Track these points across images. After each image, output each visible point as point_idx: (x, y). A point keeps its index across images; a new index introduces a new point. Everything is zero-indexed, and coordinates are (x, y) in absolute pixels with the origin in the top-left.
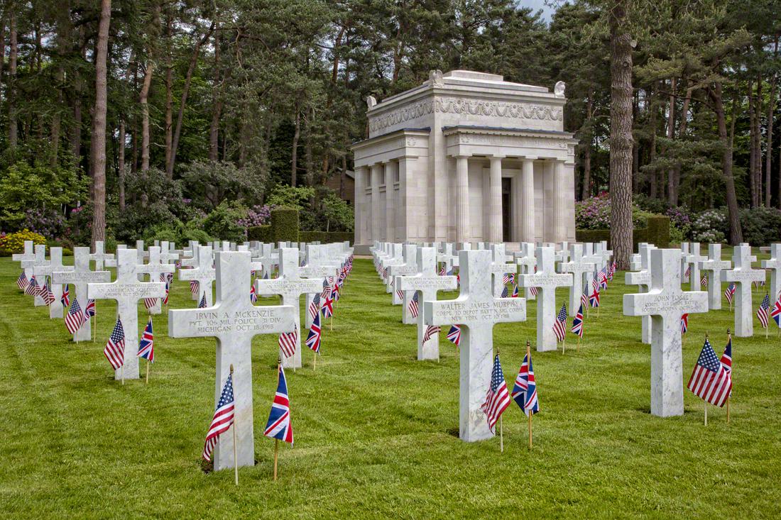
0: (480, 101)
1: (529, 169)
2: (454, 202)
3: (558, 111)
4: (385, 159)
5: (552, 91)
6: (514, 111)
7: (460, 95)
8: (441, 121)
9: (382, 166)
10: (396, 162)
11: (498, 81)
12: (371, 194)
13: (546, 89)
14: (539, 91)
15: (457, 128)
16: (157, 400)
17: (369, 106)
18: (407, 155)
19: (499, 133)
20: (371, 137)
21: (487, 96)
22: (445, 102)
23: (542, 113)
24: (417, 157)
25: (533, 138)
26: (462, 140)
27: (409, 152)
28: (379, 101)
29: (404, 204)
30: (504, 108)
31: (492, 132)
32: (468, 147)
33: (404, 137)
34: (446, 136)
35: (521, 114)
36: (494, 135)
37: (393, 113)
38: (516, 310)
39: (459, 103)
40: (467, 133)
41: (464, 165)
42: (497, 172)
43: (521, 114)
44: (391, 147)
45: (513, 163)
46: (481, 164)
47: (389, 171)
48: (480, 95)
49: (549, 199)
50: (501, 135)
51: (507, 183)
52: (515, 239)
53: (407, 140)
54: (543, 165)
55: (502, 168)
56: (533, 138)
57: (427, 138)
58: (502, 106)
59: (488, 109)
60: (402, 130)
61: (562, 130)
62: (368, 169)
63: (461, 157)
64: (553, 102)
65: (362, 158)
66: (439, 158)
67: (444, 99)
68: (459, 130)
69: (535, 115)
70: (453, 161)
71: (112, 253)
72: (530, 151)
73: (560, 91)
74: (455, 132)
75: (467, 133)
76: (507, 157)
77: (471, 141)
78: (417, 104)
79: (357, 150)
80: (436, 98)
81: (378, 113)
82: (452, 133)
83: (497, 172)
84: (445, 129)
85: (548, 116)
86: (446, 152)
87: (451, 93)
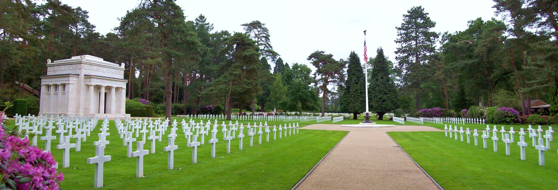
0: (98, 67)
1: (113, 90)
2: (87, 100)
3: (122, 73)
4: (58, 83)
5: (120, 66)
6: (109, 71)
7: (91, 64)
8: (83, 72)
9: (56, 86)
10: (64, 85)
11: (101, 60)
12: (50, 95)
13: (119, 65)
14: (117, 65)
15: (91, 75)
16: (482, 74)
17: (48, 62)
18: (70, 83)
19: (105, 78)
20: (48, 74)
21: (100, 66)
22: (86, 66)
23: (117, 73)
24: (73, 84)
25: (116, 80)
26: (92, 80)
27: (71, 82)
28: (52, 62)
29: (68, 100)
30: (105, 70)
31: (102, 78)
32: (94, 82)
33: (69, 77)
34: (85, 78)
35: (111, 72)
36: (105, 79)
37: (61, 67)
38: (154, 126)
39: (90, 67)
40: (94, 78)
41: (92, 88)
42: (103, 91)
43: (111, 72)
44: (66, 79)
45: (109, 88)
46: (98, 87)
47: (60, 88)
48: (98, 65)
49: (119, 100)
50: (99, 78)
51: (106, 93)
52: (107, 113)
53: (70, 77)
54: (117, 89)
55: (105, 89)
56: (116, 80)
57: (78, 77)
58: (105, 69)
59: (100, 70)
60: (69, 74)
61: (123, 78)
62: (48, 86)
63: (91, 85)
64: (121, 69)
65: (44, 82)
66: (83, 84)
67: (85, 65)
68: (92, 76)
69: (107, 72)
70: (88, 86)
71: (238, 108)
72: (114, 85)
73: (123, 65)
74: (90, 77)
75: (94, 78)
76: (107, 86)
77: (95, 80)
78: (73, 65)
79: (43, 78)
80: (83, 65)
81: (50, 66)
82: (88, 77)
83: (103, 91)
84: (85, 75)
85: (119, 74)
86: (85, 83)
87: (88, 63)
